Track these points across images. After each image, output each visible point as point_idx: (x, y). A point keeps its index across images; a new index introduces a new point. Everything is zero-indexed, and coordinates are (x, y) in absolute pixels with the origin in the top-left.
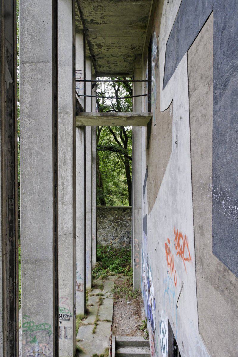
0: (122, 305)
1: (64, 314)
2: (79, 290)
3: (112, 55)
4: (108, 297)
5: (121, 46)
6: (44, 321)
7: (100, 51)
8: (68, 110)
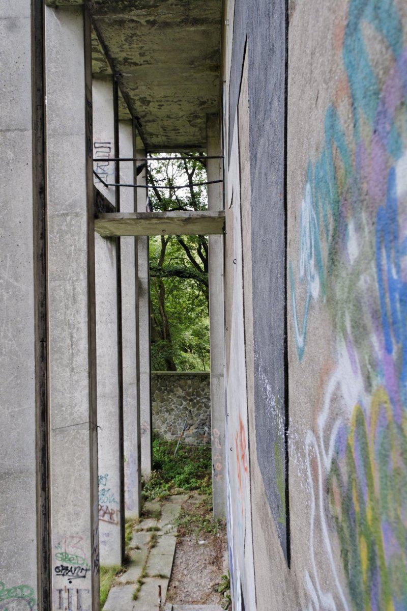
0: (190, 547)
1: (76, 566)
2: (112, 521)
3: (168, 117)
4: (167, 533)
5: (181, 101)
6: (22, 582)
7: (146, 110)
8: (78, 210)
